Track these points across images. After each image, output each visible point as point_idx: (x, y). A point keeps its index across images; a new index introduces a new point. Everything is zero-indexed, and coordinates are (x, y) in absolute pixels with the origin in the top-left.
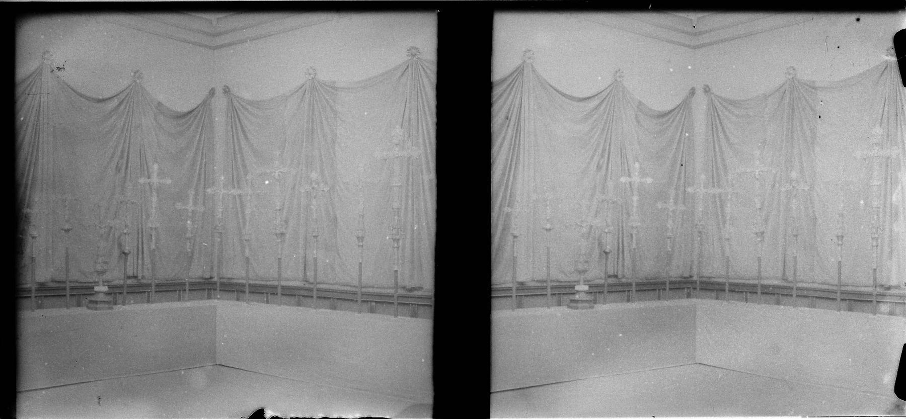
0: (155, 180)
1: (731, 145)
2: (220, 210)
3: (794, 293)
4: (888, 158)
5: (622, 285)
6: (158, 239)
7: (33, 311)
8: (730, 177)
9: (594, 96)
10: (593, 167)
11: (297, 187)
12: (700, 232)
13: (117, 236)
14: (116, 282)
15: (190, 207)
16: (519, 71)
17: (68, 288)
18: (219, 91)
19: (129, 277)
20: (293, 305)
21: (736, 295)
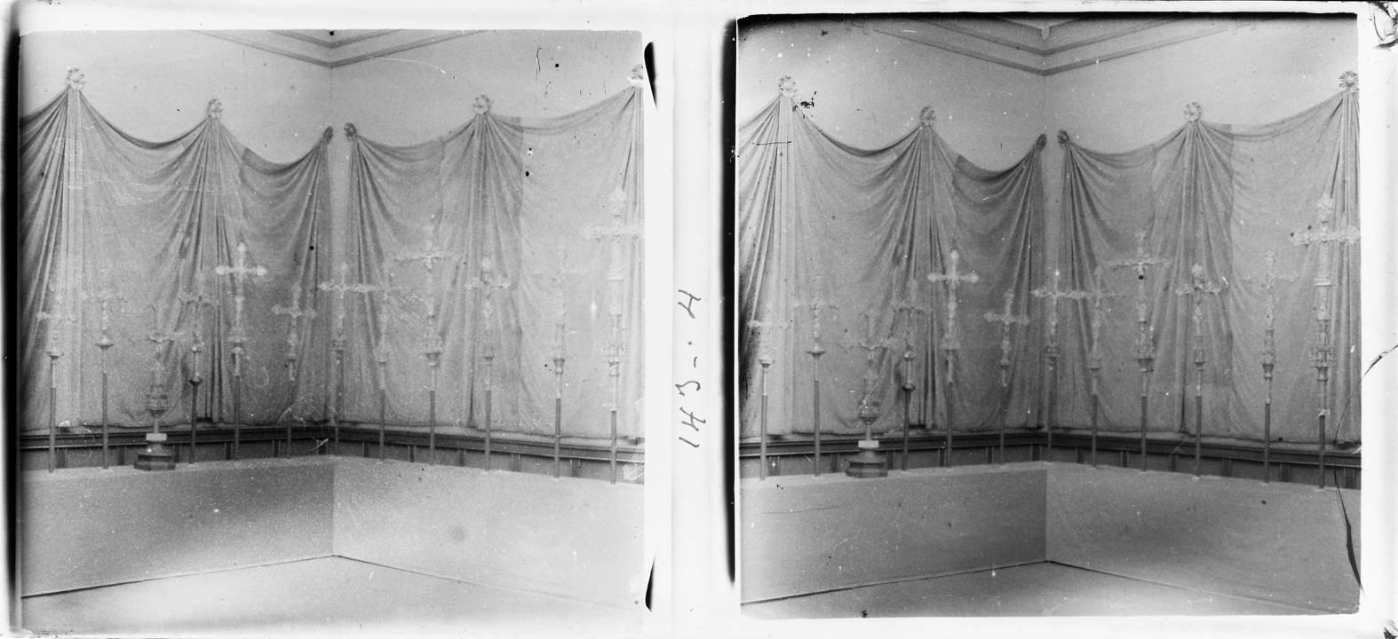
0: (953, 276)
1: (387, 216)
2: (1054, 323)
3: (487, 447)
4: (1342, 244)
5: (219, 432)
6: (957, 367)
7: (51, 471)
8: (387, 265)
9: (174, 141)
10: (174, 249)
11: (1171, 288)
12: (340, 352)
13: (893, 363)
14: (892, 434)
15: (1007, 318)
16: (62, 100)
17: (817, 443)
18: (1052, 139)
19: (912, 427)
20: (1164, 469)
21: (396, 451)
